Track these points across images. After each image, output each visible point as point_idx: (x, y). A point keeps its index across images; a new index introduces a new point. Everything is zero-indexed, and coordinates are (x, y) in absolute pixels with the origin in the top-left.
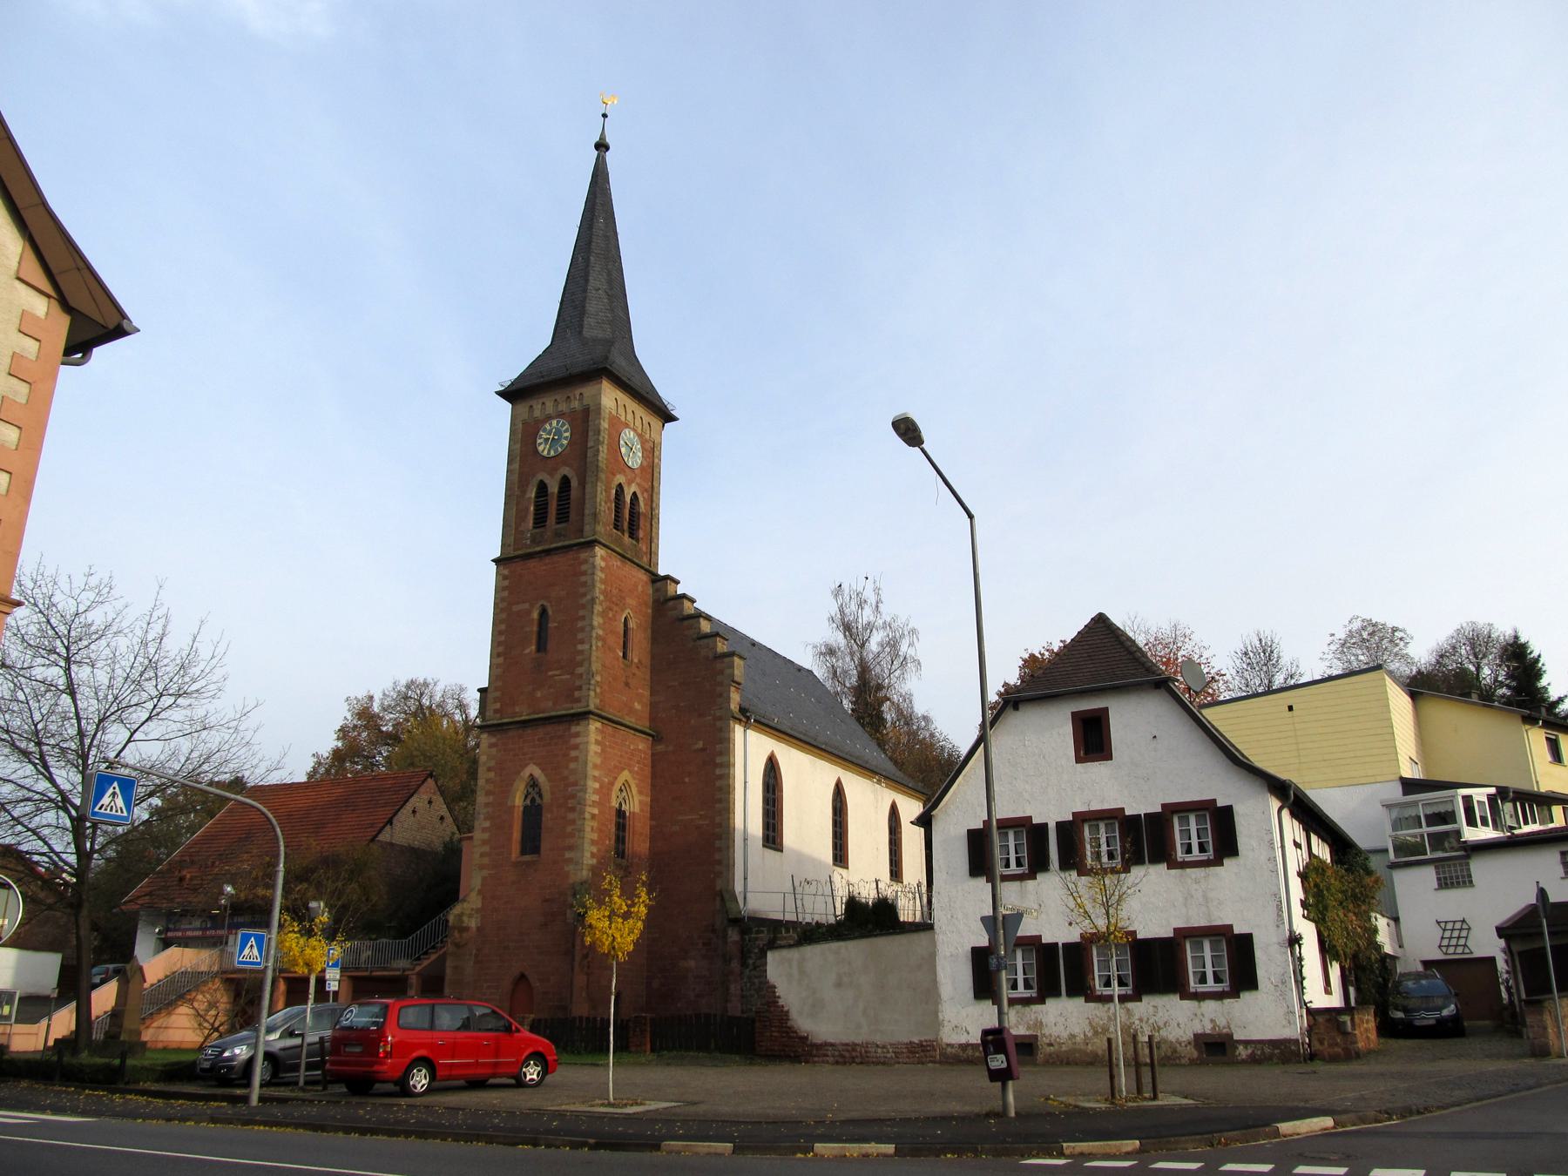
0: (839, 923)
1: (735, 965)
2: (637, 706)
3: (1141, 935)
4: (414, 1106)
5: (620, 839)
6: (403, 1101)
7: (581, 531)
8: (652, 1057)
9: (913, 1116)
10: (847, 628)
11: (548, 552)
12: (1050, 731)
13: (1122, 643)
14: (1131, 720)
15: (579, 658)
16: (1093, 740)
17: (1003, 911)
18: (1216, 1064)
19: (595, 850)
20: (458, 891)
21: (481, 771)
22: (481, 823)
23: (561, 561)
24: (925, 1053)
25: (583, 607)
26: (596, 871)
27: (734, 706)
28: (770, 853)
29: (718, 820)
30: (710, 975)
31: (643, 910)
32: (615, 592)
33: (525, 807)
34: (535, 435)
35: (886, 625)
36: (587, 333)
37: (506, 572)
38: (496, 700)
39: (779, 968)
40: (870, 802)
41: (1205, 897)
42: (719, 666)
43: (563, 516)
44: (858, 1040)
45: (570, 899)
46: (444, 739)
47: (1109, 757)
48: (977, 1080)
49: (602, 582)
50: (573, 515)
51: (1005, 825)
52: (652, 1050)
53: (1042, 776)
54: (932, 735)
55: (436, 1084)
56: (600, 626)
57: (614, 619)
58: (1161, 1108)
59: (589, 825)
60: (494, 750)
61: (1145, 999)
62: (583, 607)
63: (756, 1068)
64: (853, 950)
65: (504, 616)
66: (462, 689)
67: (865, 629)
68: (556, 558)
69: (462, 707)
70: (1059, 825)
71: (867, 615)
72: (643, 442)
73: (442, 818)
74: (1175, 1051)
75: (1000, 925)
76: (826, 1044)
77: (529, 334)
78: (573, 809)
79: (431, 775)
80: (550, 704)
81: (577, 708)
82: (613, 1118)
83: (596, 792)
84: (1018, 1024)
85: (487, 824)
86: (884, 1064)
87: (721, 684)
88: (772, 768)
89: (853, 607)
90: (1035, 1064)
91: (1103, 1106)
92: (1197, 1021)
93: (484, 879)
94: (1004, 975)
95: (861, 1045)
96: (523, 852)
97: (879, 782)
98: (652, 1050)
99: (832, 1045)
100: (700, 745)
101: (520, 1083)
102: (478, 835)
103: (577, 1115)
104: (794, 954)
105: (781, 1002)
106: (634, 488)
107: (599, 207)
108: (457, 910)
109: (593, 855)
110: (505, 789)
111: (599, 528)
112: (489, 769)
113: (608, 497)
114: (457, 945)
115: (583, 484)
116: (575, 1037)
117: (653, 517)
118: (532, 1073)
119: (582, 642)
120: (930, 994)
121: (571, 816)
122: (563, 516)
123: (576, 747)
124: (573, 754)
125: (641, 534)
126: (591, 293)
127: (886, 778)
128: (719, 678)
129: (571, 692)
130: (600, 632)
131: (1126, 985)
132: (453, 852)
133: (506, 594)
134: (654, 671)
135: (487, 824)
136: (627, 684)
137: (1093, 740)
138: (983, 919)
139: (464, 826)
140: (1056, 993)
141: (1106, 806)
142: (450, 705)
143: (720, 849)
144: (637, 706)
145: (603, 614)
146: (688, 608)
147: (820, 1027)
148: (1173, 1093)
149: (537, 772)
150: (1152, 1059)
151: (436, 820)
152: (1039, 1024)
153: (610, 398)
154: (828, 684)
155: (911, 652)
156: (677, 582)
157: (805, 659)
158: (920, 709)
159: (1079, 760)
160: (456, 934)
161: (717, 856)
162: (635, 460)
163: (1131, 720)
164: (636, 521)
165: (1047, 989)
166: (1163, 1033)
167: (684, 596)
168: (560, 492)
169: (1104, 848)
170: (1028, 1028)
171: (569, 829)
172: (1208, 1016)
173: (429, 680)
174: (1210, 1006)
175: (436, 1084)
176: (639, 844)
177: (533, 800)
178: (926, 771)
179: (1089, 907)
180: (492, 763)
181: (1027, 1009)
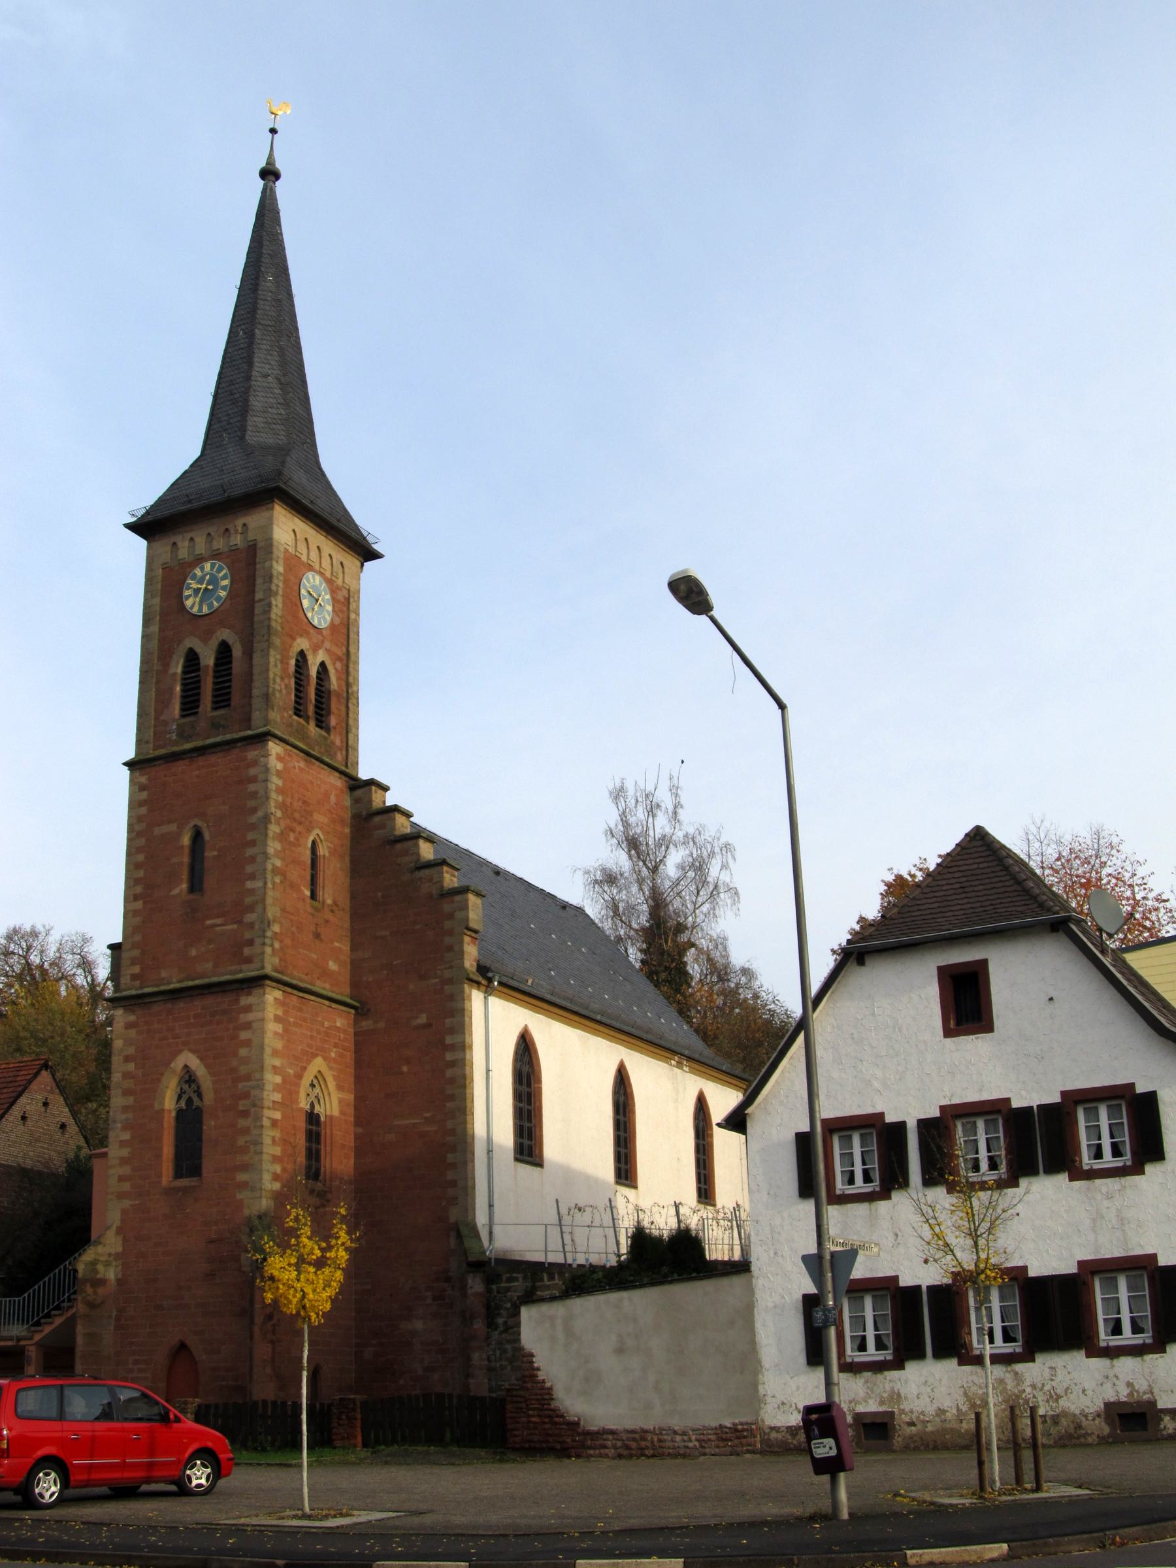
0: (621, 1266)
1: (479, 1325)
2: (333, 966)
3: (1035, 1270)
4: (43, 1521)
5: (313, 1155)
6: (27, 1515)
7: (247, 721)
8: (364, 1453)
9: (712, 1522)
10: (633, 844)
11: (201, 751)
12: (910, 993)
13: (1006, 868)
14: (1020, 976)
15: (248, 900)
16: (967, 1004)
17: (831, 1247)
18: (1132, 1441)
19: (278, 1168)
20: (88, 1228)
21: (116, 1060)
22: (118, 1135)
23: (220, 763)
24: (739, 1440)
25: (253, 827)
26: (280, 1198)
27: (469, 964)
28: (525, 1170)
29: (449, 1124)
30: (441, 1335)
31: (343, 1255)
32: (297, 805)
33: (180, 1112)
34: (181, 584)
35: (689, 839)
36: (251, 438)
37: (143, 780)
38: (134, 962)
39: (539, 1330)
40: (668, 1094)
41: (1122, 1220)
42: (447, 907)
43: (222, 698)
44: (649, 1425)
45: (245, 1238)
46: (63, 1014)
47: (989, 1028)
48: (800, 1473)
49: (280, 791)
50: (236, 699)
51: (840, 1127)
52: (365, 1445)
53: (893, 1057)
54: (756, 996)
55: (71, 1492)
56: (277, 854)
57: (296, 844)
58: (1045, 1502)
59: (269, 1135)
60: (132, 1033)
61: (1040, 1358)
62: (253, 827)
63: (507, 1466)
64: (640, 1303)
65: (142, 841)
66: (86, 940)
67: (658, 844)
68: (213, 759)
69: (86, 965)
70: (924, 1124)
71: (661, 826)
72: (333, 588)
73: (63, 1126)
74: (1079, 1427)
75: (827, 1266)
76: (606, 1432)
77: (170, 443)
78: (245, 1114)
79: (46, 1066)
80: (209, 965)
81: (249, 972)
82: (308, 1533)
83: (277, 1088)
84: (857, 1396)
85: (126, 1136)
86: (684, 1456)
87: (450, 933)
88: (525, 1050)
89: (641, 814)
90: (890, 1450)
91: (967, 1501)
92: (1108, 1385)
93: (124, 1212)
94: (832, 1331)
95: (653, 1432)
96: (178, 1175)
97: (679, 1065)
98: (365, 1445)
99: (612, 1432)
100: (423, 1019)
101: (183, 1490)
102: (115, 1151)
103: (260, 1530)
104: (558, 1310)
105: (541, 1376)
106: (321, 656)
107: (266, 260)
108: (89, 1255)
109: (276, 1177)
110: (148, 1087)
111: (274, 715)
112: (127, 1059)
113: (285, 670)
114: (92, 1305)
115: (249, 653)
116: (255, 1428)
117: (349, 697)
118: (199, 1476)
119: (252, 877)
120: (747, 1361)
121: (242, 1123)
122: (222, 698)
123: (248, 1026)
124: (244, 1035)
125: (333, 721)
126: (257, 381)
127: (690, 1058)
128: (448, 924)
129: (240, 947)
130: (278, 863)
131: (1014, 1340)
132: (79, 1177)
133: (144, 810)
134: (356, 914)
135: (126, 1136)
136: (317, 936)
137: (967, 1004)
138: (806, 1259)
139: (95, 1136)
140: (918, 1354)
141: (986, 1096)
142: (70, 963)
143: (453, 1166)
144: (333, 966)
145: (282, 837)
146: (402, 825)
147: (577, 1403)
148: (1066, 1483)
149: (194, 1062)
150: (1034, 1439)
151: (54, 1128)
152: (896, 1397)
153: (286, 529)
154: (607, 926)
155: (725, 877)
156: (385, 789)
157: (572, 889)
158: (738, 958)
159: (948, 1033)
160: (89, 1290)
161: (450, 1175)
162: (321, 615)
163: (1020, 976)
164: (325, 703)
165: (906, 1348)
166: (1063, 1403)
167: (395, 809)
168: (217, 664)
169: (983, 1154)
170: (882, 1403)
171: (241, 1141)
172: (1125, 1376)
173: (39, 928)
174: (1126, 1365)
175: (71, 1492)
176: (340, 1160)
177: (189, 1101)
178: (741, 1042)
179: (951, 1239)
180: (131, 1051)
181: (879, 1376)
